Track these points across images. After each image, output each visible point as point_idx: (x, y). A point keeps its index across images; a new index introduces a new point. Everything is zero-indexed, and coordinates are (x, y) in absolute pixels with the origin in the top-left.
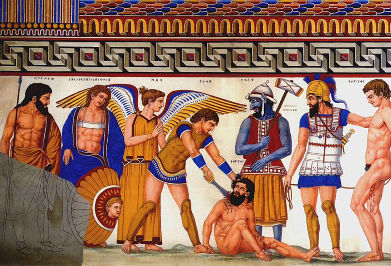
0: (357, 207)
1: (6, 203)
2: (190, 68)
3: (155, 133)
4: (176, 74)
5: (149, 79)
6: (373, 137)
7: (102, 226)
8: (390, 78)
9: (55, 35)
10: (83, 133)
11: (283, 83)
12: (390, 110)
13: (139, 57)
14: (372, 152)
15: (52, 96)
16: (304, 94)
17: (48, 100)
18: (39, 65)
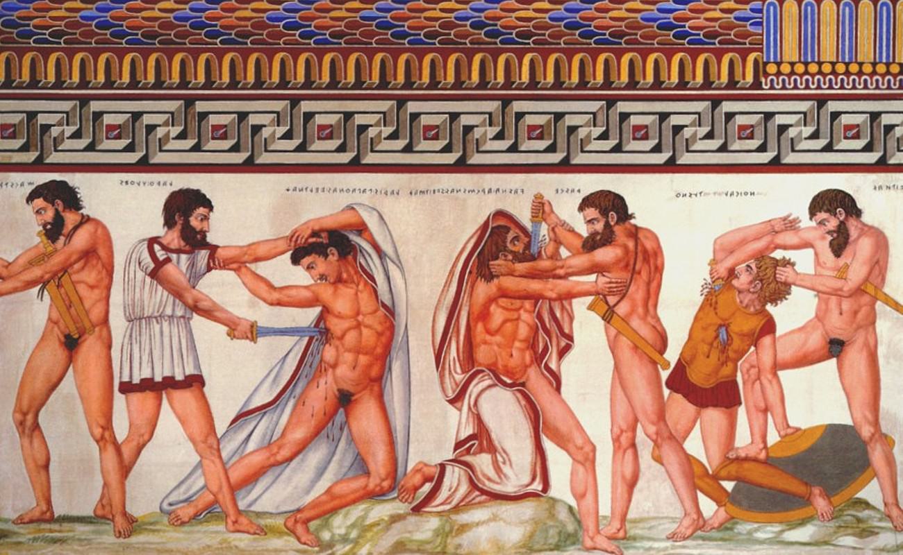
2: (695, 154)
9: (893, 87)
17: (205, 223)
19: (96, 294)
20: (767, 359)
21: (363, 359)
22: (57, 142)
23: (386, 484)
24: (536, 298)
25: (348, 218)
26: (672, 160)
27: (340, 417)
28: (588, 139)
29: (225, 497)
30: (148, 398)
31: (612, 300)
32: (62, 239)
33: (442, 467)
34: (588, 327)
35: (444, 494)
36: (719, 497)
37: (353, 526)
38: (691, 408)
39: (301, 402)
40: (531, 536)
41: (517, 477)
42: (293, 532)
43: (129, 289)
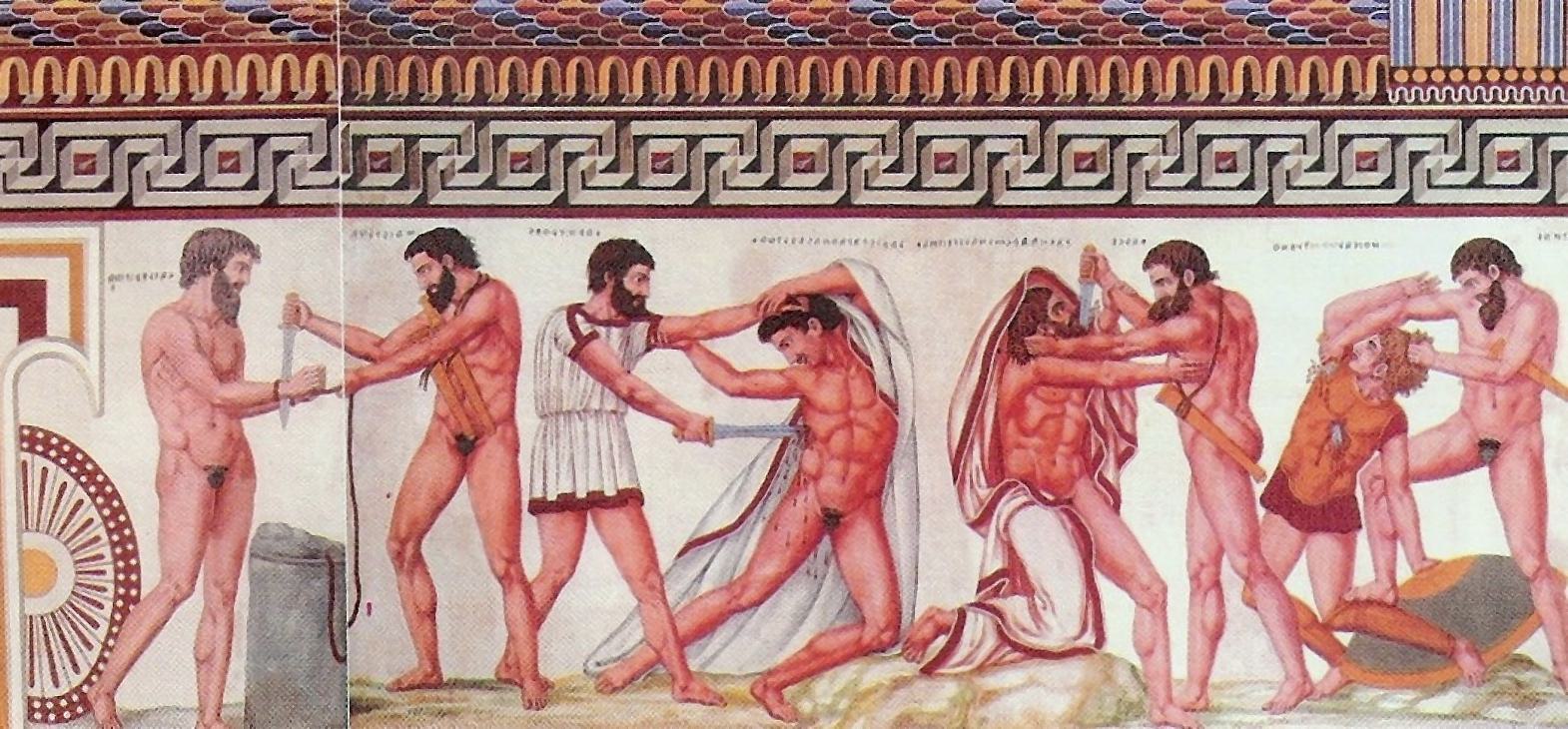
8: (1566, 220)
12: (1566, 405)
21: (855, 469)
23: (886, 637)
24: (1086, 386)
29: (671, 653)
31: (1188, 389)
32: (452, 308)
33: (962, 614)
36: (1333, 654)
37: (842, 694)
38: (1294, 534)
41: (1062, 625)
43: (542, 375)
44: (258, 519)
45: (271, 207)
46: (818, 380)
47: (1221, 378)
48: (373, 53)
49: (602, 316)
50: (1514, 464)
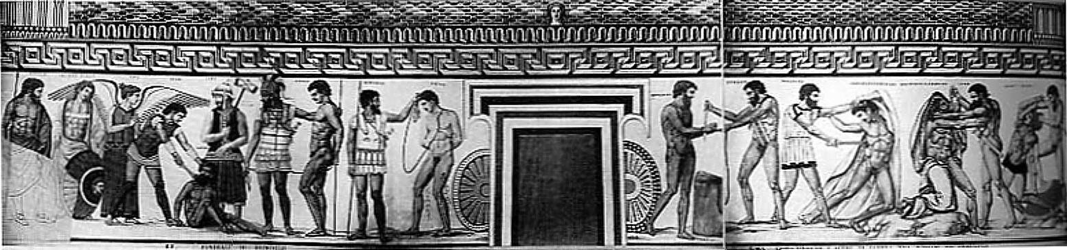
0: (305, 189)
1: (56, 200)
3: (132, 123)
4: (151, 72)
5: (128, 76)
6: (316, 129)
7: (85, 200)
10: (71, 122)
11: (240, 82)
13: (206, 60)
14: (316, 141)
15: (45, 89)
16: (258, 92)
18: (34, 63)
19: (772, 127)
20: (1036, 154)
21: (882, 154)
22: (928, 64)
23: (891, 207)
24: (952, 128)
25: (877, 95)
26: (879, 71)
27: (872, 178)
28: (758, 63)
29: (825, 212)
30: (794, 170)
31: (982, 129)
32: (758, 105)
33: (914, 199)
34: (972, 138)
35: (915, 211)
36: (1022, 211)
37: (878, 224)
38: (1011, 174)
39: (856, 173)
40: (950, 228)
41: (945, 203)
42: (853, 227)
43: (787, 126)
44: (697, 169)
45: (700, 74)
46: (870, 127)
47: (991, 126)
48: (735, 26)
49: (804, 108)
50: (1059, 151)
